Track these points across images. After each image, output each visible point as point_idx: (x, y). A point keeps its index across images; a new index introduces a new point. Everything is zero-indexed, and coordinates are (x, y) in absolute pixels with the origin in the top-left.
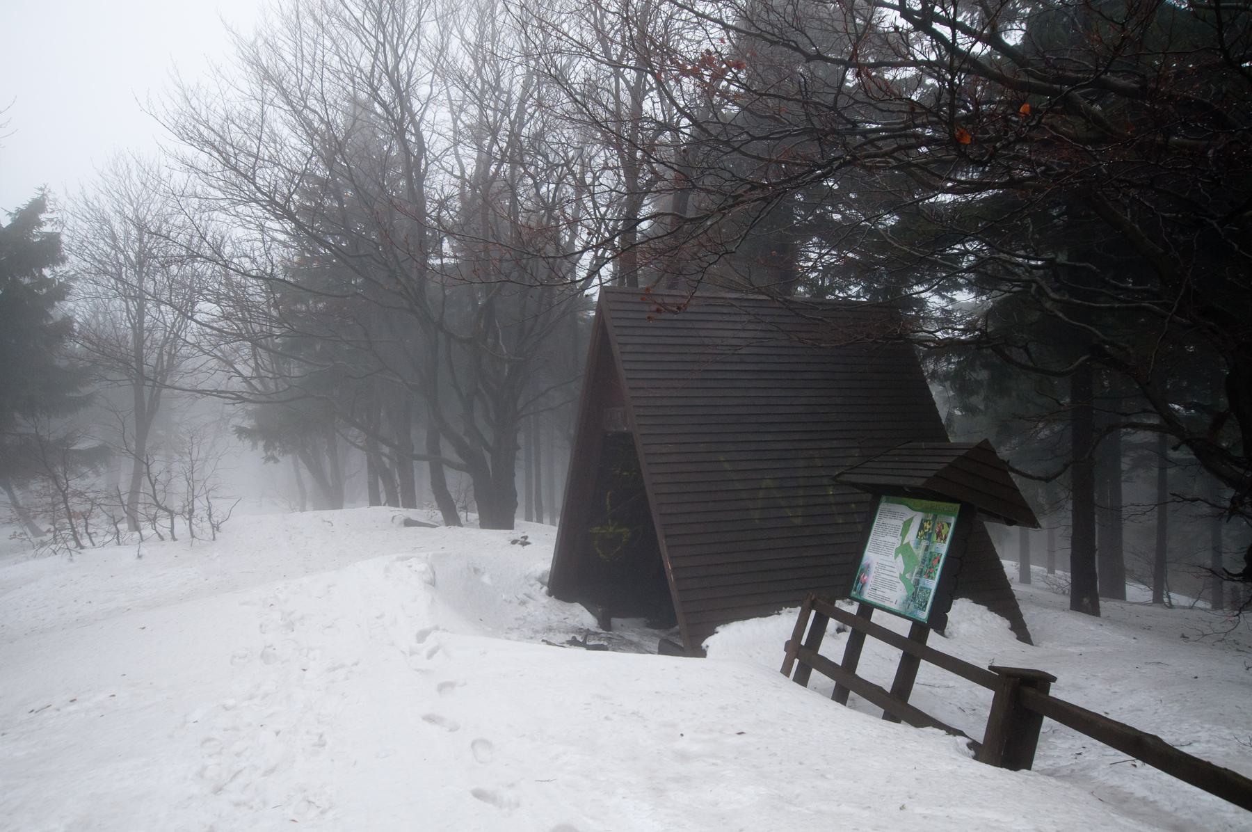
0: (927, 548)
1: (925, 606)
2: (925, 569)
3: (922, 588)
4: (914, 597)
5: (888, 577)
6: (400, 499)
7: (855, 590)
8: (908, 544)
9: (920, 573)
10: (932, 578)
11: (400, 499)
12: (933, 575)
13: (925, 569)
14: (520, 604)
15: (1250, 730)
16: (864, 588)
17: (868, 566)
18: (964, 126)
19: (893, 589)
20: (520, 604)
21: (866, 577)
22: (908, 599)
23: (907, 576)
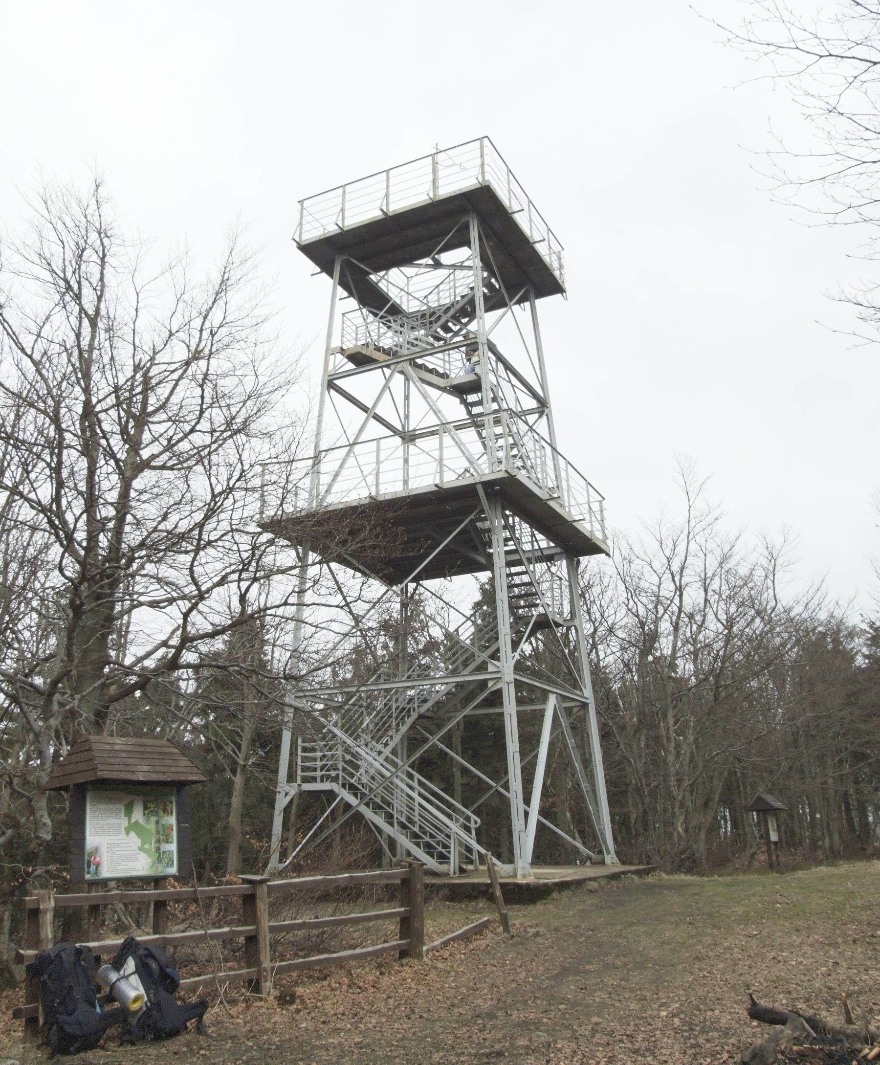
0: (157, 822)
1: (173, 863)
2: (162, 837)
3: (164, 853)
4: (159, 860)
5: (122, 853)
6: (403, 942)
7: (89, 873)
8: (137, 822)
9: (158, 841)
10: (172, 842)
11: (403, 942)
12: (170, 840)
13: (162, 837)
14: (592, 548)
15: (878, 647)
16: (100, 868)
17: (97, 849)
18: (549, 595)
19: (137, 859)
20: (592, 548)
21: (98, 859)
22: (154, 864)
23: (147, 846)
